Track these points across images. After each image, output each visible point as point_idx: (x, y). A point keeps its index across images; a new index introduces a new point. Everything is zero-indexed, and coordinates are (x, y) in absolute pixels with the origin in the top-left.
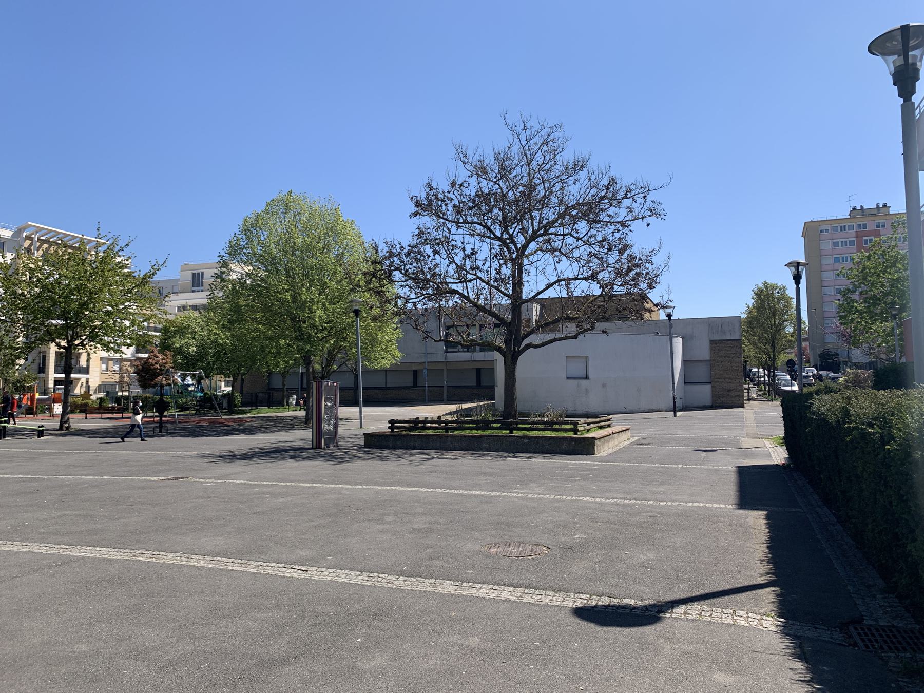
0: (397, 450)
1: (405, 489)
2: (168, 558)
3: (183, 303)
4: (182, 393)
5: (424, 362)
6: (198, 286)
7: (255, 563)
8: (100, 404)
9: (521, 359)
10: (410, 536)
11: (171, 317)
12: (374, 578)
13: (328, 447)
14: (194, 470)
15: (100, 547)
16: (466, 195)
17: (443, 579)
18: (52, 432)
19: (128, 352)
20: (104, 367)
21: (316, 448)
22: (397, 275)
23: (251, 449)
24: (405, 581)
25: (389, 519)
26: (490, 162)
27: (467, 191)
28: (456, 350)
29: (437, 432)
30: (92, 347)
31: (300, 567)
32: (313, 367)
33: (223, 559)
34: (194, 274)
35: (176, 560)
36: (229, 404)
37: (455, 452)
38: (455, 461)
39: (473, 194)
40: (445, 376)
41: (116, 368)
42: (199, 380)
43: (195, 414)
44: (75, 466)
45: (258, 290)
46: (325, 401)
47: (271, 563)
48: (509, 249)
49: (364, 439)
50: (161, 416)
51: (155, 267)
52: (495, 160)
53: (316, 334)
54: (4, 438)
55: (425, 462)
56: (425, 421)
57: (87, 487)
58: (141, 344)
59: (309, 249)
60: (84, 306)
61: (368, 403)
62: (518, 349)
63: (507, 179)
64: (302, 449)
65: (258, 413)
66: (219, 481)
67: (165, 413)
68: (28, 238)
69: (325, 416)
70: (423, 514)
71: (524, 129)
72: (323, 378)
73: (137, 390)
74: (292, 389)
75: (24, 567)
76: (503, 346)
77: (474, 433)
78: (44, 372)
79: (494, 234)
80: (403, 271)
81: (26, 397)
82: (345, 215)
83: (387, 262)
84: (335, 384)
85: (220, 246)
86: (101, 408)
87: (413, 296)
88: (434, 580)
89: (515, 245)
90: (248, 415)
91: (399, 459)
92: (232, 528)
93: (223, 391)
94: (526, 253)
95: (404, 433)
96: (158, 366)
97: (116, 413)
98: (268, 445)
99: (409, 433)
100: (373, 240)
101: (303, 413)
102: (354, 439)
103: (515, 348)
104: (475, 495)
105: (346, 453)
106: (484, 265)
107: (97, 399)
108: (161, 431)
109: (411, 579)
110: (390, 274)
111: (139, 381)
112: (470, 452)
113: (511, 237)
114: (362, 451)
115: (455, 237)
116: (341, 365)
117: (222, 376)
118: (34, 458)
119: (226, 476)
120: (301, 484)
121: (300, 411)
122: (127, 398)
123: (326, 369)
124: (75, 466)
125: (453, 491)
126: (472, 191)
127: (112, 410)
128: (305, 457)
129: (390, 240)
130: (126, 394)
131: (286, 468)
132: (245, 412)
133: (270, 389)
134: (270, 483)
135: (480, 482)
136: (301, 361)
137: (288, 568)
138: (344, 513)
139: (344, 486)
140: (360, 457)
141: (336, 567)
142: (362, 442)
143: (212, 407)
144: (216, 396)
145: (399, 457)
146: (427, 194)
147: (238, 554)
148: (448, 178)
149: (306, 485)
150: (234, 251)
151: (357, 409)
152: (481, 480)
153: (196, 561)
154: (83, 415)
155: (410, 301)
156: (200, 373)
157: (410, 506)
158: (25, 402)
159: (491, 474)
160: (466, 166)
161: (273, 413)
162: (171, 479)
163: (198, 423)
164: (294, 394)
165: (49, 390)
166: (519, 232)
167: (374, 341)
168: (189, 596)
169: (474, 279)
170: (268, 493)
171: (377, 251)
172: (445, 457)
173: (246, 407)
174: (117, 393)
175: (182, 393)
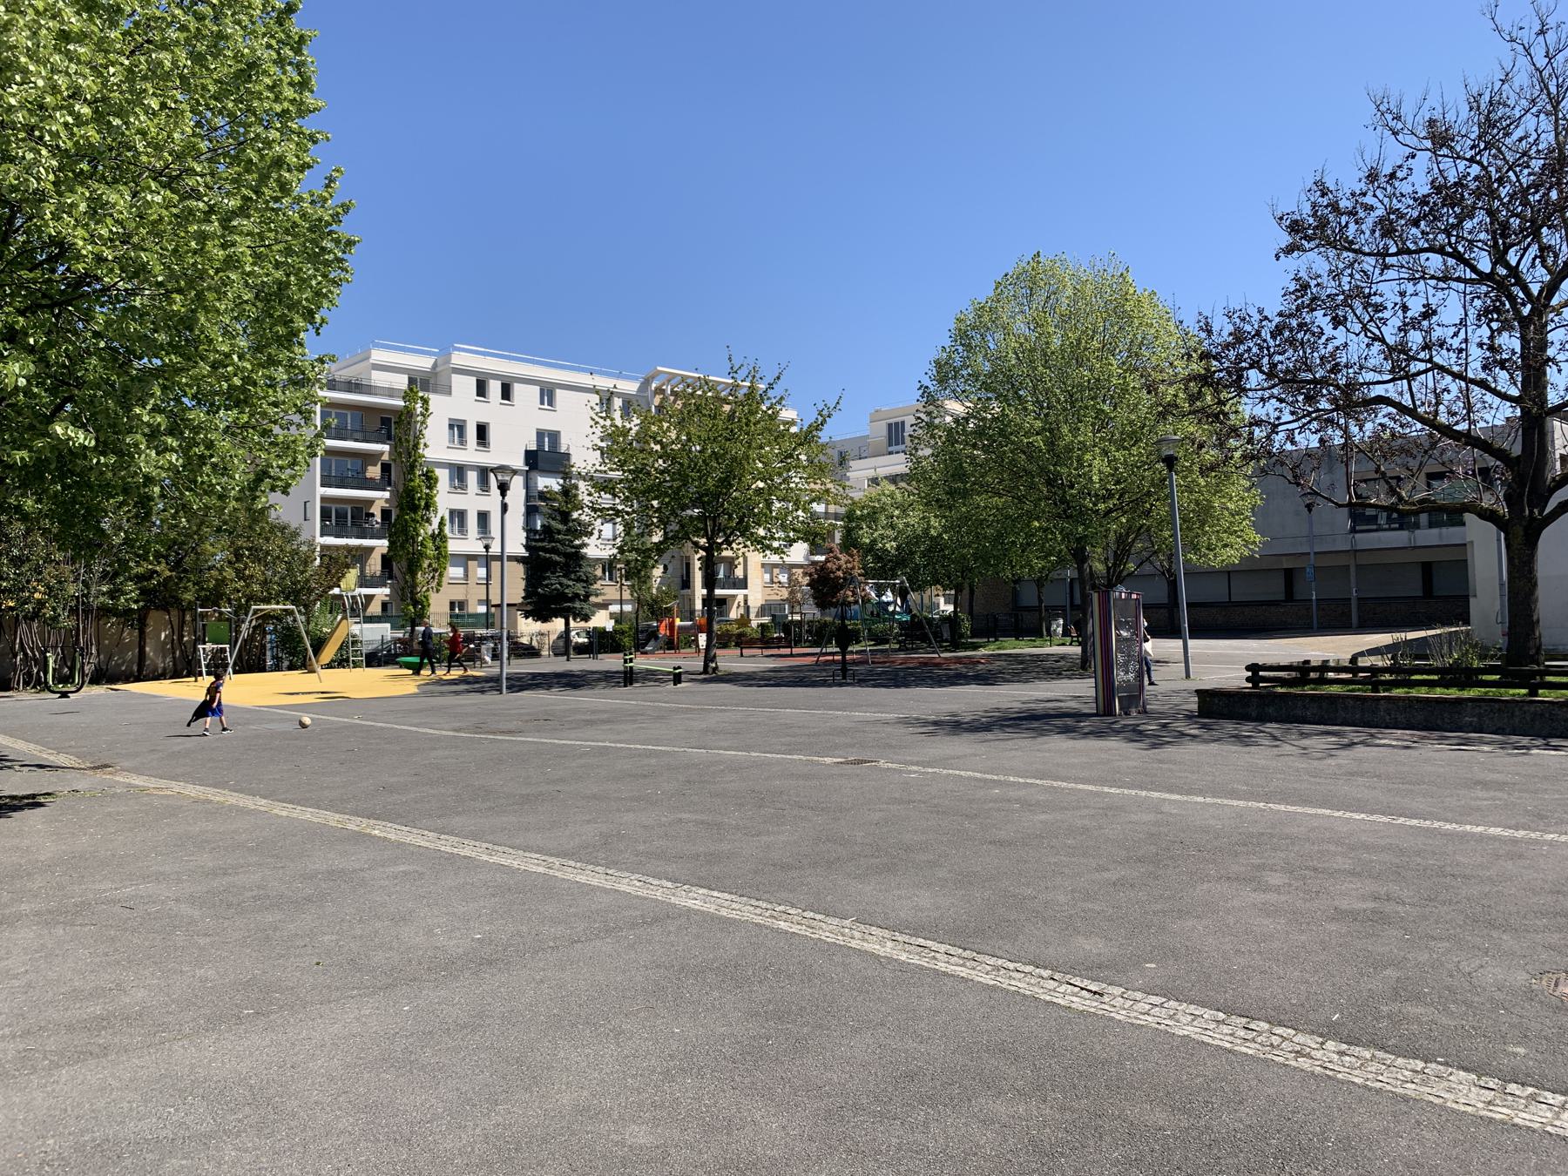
0: (1268, 725)
1: (1299, 809)
2: (829, 930)
3: (871, 473)
4: (878, 615)
5: (1309, 554)
6: (897, 444)
7: (992, 961)
8: (762, 633)
9: (1546, 533)
10: (1333, 927)
11: (857, 496)
12: (1260, 1033)
13: (1126, 714)
14: (890, 746)
15: (719, 891)
16: (1403, 195)
17: (1446, 1064)
18: (693, 677)
19: (799, 552)
20: (767, 577)
21: (1104, 715)
22: (1254, 377)
23: (986, 711)
24: (1342, 1053)
25: (1275, 879)
26: (1460, 117)
27: (1405, 188)
28: (1375, 527)
29: (1353, 690)
30: (741, 546)
31: (1086, 983)
32: (1091, 567)
33: (929, 943)
34: (890, 425)
35: (843, 935)
36: (948, 633)
37: (1399, 732)
38: (1409, 751)
39: (1424, 190)
40: (1353, 579)
41: (784, 578)
42: (902, 593)
43: (899, 650)
44: (714, 732)
45: (991, 434)
46: (1116, 628)
47: (1024, 964)
48: (1512, 299)
49: (1196, 699)
50: (844, 653)
51: (824, 413)
52: (1471, 109)
53: (1095, 505)
54: (631, 684)
55: (1333, 752)
56: (1324, 667)
57: (723, 771)
58: (814, 538)
59: (1076, 354)
60: (725, 482)
61: (1200, 632)
62: (1541, 513)
63: (1499, 150)
64: (1079, 716)
65: (998, 649)
66: (930, 770)
67: (850, 649)
68: (660, 391)
69: (1119, 658)
70: (1353, 873)
71: (1542, 32)
72: (1111, 585)
73: (811, 611)
74: (1055, 608)
75: (595, 921)
76: (1503, 509)
77: (1438, 693)
78: (689, 588)
79: (1474, 269)
80: (1265, 369)
81: (664, 623)
82: (1139, 284)
83: (1232, 354)
84: (1134, 596)
85: (923, 372)
86: (764, 640)
87: (1287, 417)
88: (1420, 1065)
89: (1525, 289)
90: (983, 651)
91: (1278, 743)
92: (950, 871)
93: (943, 611)
94: (1554, 302)
95: (1279, 690)
96: (840, 574)
97: (783, 647)
98: (1017, 705)
99: (1292, 690)
100: (1200, 314)
101: (1078, 650)
102: (1176, 700)
103: (1531, 512)
104: (1473, 834)
105: (1164, 726)
106: (1456, 334)
107: (758, 626)
108: (844, 678)
109: (1357, 1050)
110: (1240, 377)
111: (815, 598)
112: (1436, 734)
113: (1514, 271)
114: (1196, 723)
115: (1382, 287)
116: (1141, 564)
117: (939, 587)
118: (662, 717)
119: (943, 762)
120: (1081, 786)
121: (1071, 645)
122: (799, 624)
123: (1115, 570)
124: (714, 732)
125: (1414, 822)
126: (1419, 182)
127: (777, 643)
128: (1086, 730)
129: (1238, 308)
130: (797, 617)
131: (1049, 751)
132: (975, 647)
133: (1017, 608)
134: (1021, 780)
135: (1479, 803)
136: (1069, 557)
137: (1061, 983)
138: (1172, 858)
139: (1167, 796)
140: (1194, 736)
141: (1168, 994)
142: (1193, 704)
143: (924, 638)
144: (930, 621)
145: (1275, 738)
146: (1314, 205)
147: (962, 936)
148: (1361, 164)
149: (1090, 788)
150: (945, 373)
151: (1180, 643)
152: (1478, 798)
153: (881, 944)
154: (738, 651)
155: (1280, 428)
156: (902, 582)
157: (1319, 852)
158: (663, 632)
159: (1500, 786)
160: (1400, 137)
161: (1025, 648)
162: (852, 763)
163: (901, 664)
164: (1058, 616)
165: (697, 613)
166: (1536, 257)
167: (1204, 512)
168: (855, 1031)
169: (1426, 371)
170: (1018, 801)
171: (1209, 332)
172: (1378, 741)
173: (981, 637)
174: (787, 616)
175: (878, 615)
